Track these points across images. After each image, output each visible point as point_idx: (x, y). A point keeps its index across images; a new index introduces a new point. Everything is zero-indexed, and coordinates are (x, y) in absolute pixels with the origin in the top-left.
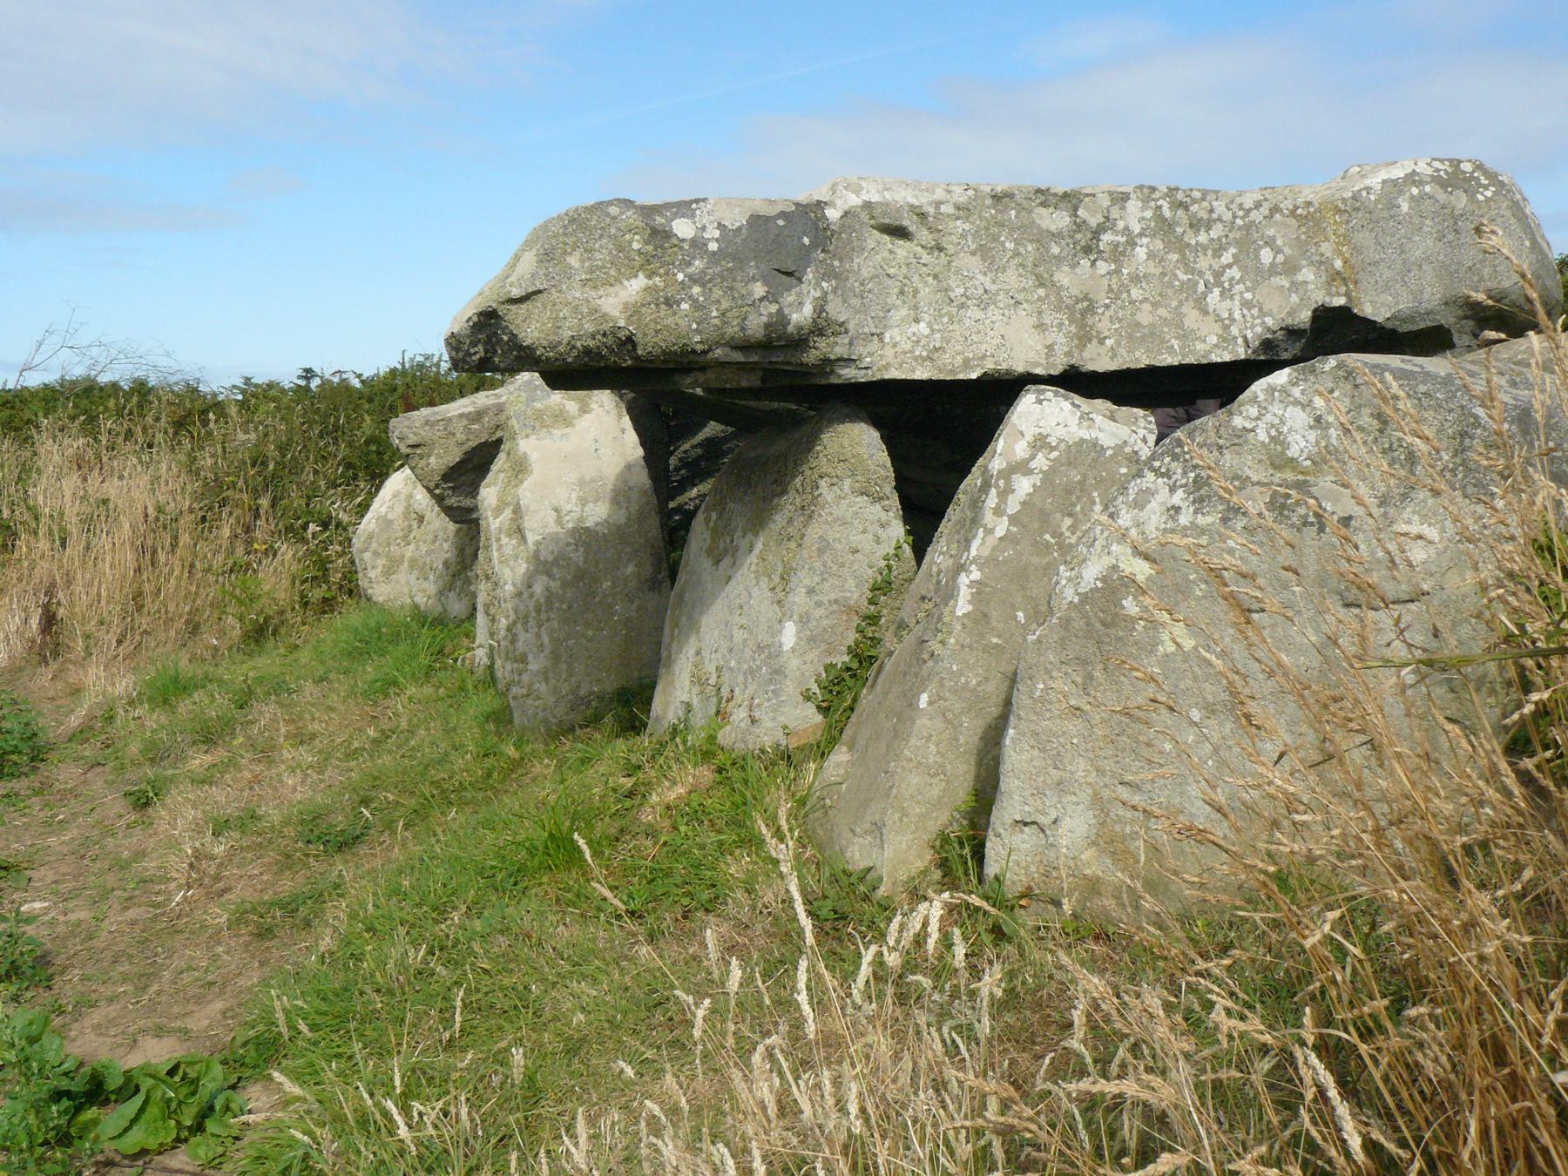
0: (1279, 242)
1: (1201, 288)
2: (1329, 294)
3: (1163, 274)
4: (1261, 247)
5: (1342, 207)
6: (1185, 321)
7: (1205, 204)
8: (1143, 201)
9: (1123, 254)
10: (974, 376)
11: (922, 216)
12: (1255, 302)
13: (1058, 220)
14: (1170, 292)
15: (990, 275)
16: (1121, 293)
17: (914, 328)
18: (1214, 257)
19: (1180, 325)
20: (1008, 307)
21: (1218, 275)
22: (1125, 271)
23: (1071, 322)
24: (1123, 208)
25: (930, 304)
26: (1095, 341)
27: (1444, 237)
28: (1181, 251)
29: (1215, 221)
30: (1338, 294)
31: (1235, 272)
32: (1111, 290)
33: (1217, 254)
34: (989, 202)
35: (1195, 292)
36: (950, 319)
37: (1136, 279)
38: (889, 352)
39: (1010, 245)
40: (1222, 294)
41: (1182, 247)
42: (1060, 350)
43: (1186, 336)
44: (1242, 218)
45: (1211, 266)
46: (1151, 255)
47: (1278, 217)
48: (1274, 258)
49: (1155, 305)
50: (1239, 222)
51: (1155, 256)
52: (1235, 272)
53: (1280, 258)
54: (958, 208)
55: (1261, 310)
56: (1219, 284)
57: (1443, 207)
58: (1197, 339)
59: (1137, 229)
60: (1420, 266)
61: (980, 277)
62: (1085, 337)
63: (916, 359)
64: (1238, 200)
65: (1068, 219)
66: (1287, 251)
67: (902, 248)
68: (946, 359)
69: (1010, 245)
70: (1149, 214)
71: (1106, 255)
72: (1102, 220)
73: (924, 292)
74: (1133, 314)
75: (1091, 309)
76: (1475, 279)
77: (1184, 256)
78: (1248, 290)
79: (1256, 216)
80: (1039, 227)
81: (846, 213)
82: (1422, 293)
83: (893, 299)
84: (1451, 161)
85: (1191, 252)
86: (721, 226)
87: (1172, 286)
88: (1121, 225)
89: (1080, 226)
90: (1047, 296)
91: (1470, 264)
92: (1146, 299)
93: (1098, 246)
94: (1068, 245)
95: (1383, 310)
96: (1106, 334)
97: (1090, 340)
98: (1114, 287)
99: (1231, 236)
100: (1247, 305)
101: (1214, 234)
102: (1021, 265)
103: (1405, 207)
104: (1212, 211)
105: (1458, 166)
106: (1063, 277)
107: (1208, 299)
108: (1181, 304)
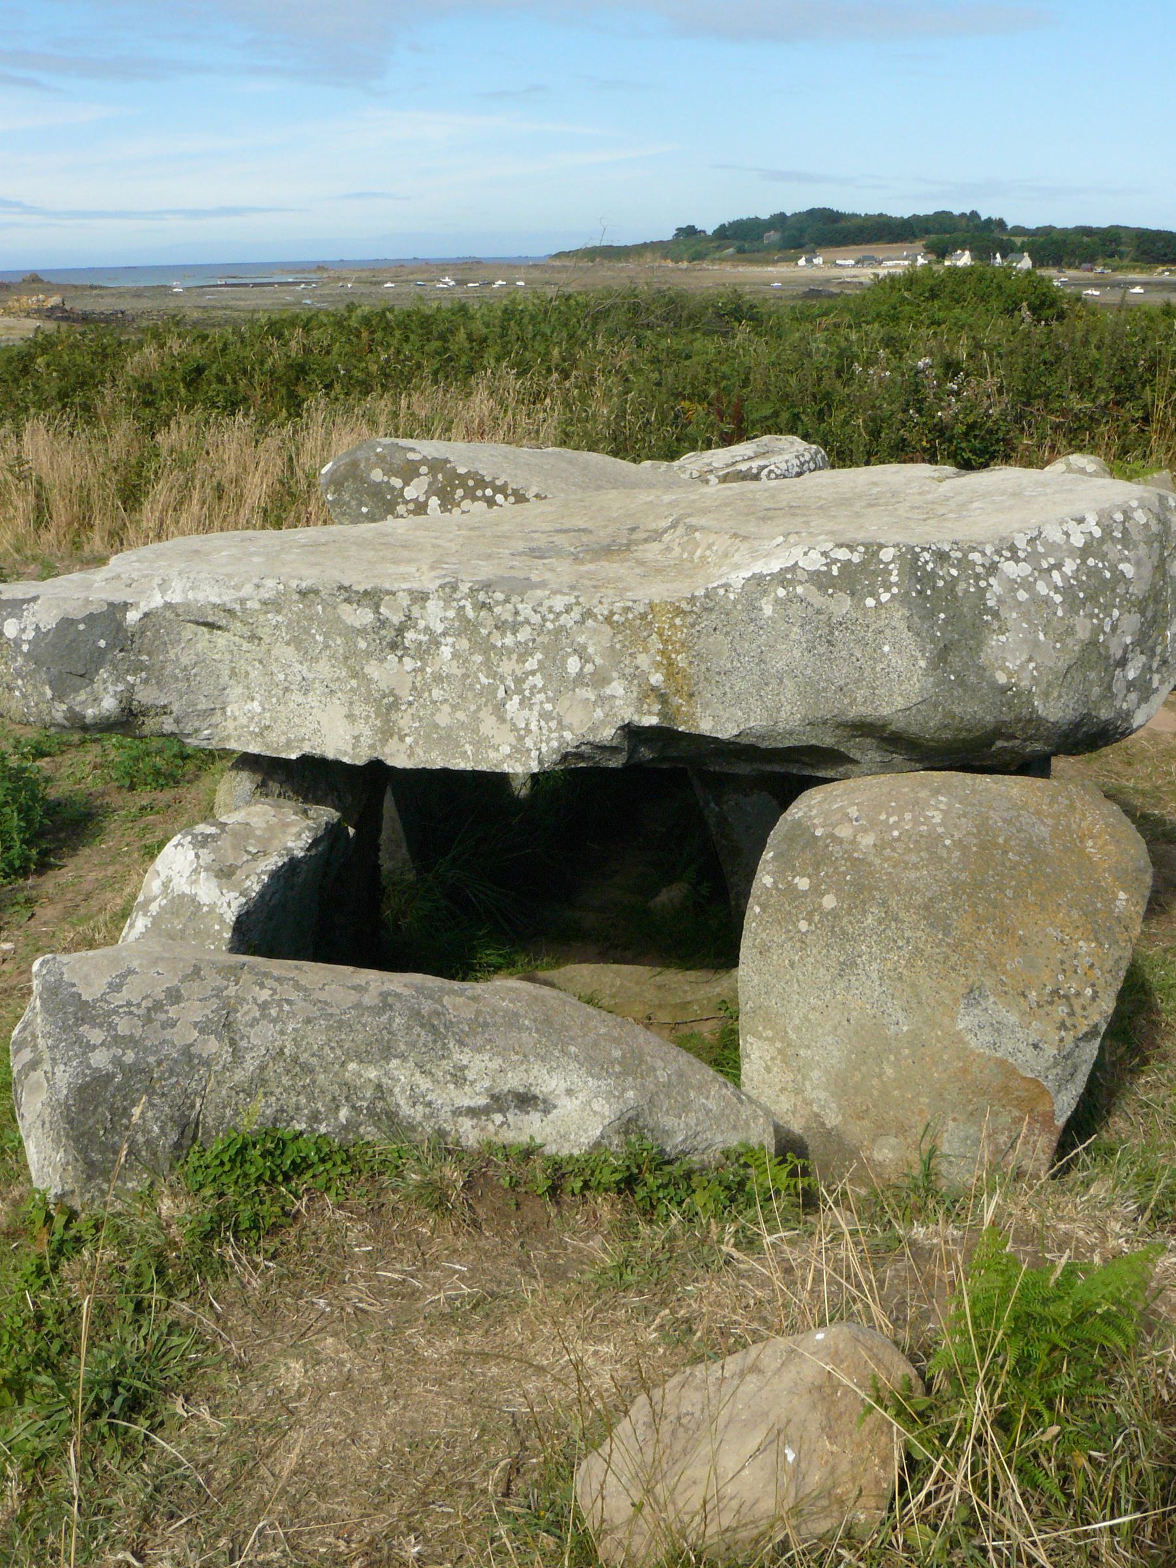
0: (591, 650)
1: (501, 694)
2: (639, 710)
3: (466, 676)
4: (569, 655)
5: (687, 608)
6: (481, 727)
7: (509, 606)
8: (445, 601)
9: (427, 651)
10: (293, 757)
11: (230, 612)
12: (554, 714)
13: (363, 617)
14: (470, 695)
15: (306, 664)
16: (423, 691)
17: (248, 706)
18: (517, 662)
19: (476, 731)
20: (323, 694)
21: (519, 681)
22: (428, 670)
23: (377, 716)
24: (424, 608)
25: (260, 685)
26: (396, 737)
27: (815, 648)
28: (485, 653)
29: (522, 624)
30: (650, 713)
31: (538, 680)
32: (414, 688)
33: (522, 659)
34: (296, 597)
35: (495, 697)
36: (278, 700)
37: (438, 679)
38: (230, 724)
39: (320, 638)
40: (521, 702)
41: (486, 648)
42: (365, 741)
43: (481, 743)
44: (553, 621)
45: (513, 671)
46: (455, 655)
47: (590, 623)
48: (581, 669)
49: (455, 708)
50: (549, 625)
51: (460, 656)
52: (538, 680)
53: (589, 668)
54: (265, 603)
55: (560, 723)
56: (520, 691)
57: (819, 612)
58: (490, 747)
59: (439, 628)
60: (781, 680)
61: (299, 667)
62: (387, 732)
63: (252, 733)
64: (547, 603)
65: (372, 615)
66: (598, 661)
67: (221, 639)
68: (272, 737)
69: (320, 638)
70: (451, 614)
71: (412, 652)
72: (403, 619)
73: (254, 674)
74: (433, 714)
75: (395, 705)
76: (846, 701)
77: (488, 659)
78: (548, 700)
79: (566, 620)
80: (343, 622)
81: (146, 615)
82: (779, 711)
83: (224, 679)
84: (867, 546)
85: (496, 654)
86: (37, 628)
87: (471, 687)
88: (422, 624)
89: (383, 623)
90: (359, 686)
91: (842, 683)
92: (446, 701)
93: (403, 643)
94: (374, 640)
95: (729, 726)
96: (407, 731)
97: (392, 736)
98: (418, 684)
99: (539, 640)
100: (545, 716)
101: (521, 637)
102: (333, 656)
103: (768, 610)
104: (517, 613)
105: (875, 554)
106: (372, 670)
107: (507, 706)
108: (479, 709)
